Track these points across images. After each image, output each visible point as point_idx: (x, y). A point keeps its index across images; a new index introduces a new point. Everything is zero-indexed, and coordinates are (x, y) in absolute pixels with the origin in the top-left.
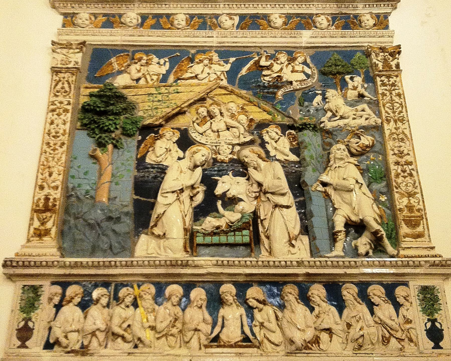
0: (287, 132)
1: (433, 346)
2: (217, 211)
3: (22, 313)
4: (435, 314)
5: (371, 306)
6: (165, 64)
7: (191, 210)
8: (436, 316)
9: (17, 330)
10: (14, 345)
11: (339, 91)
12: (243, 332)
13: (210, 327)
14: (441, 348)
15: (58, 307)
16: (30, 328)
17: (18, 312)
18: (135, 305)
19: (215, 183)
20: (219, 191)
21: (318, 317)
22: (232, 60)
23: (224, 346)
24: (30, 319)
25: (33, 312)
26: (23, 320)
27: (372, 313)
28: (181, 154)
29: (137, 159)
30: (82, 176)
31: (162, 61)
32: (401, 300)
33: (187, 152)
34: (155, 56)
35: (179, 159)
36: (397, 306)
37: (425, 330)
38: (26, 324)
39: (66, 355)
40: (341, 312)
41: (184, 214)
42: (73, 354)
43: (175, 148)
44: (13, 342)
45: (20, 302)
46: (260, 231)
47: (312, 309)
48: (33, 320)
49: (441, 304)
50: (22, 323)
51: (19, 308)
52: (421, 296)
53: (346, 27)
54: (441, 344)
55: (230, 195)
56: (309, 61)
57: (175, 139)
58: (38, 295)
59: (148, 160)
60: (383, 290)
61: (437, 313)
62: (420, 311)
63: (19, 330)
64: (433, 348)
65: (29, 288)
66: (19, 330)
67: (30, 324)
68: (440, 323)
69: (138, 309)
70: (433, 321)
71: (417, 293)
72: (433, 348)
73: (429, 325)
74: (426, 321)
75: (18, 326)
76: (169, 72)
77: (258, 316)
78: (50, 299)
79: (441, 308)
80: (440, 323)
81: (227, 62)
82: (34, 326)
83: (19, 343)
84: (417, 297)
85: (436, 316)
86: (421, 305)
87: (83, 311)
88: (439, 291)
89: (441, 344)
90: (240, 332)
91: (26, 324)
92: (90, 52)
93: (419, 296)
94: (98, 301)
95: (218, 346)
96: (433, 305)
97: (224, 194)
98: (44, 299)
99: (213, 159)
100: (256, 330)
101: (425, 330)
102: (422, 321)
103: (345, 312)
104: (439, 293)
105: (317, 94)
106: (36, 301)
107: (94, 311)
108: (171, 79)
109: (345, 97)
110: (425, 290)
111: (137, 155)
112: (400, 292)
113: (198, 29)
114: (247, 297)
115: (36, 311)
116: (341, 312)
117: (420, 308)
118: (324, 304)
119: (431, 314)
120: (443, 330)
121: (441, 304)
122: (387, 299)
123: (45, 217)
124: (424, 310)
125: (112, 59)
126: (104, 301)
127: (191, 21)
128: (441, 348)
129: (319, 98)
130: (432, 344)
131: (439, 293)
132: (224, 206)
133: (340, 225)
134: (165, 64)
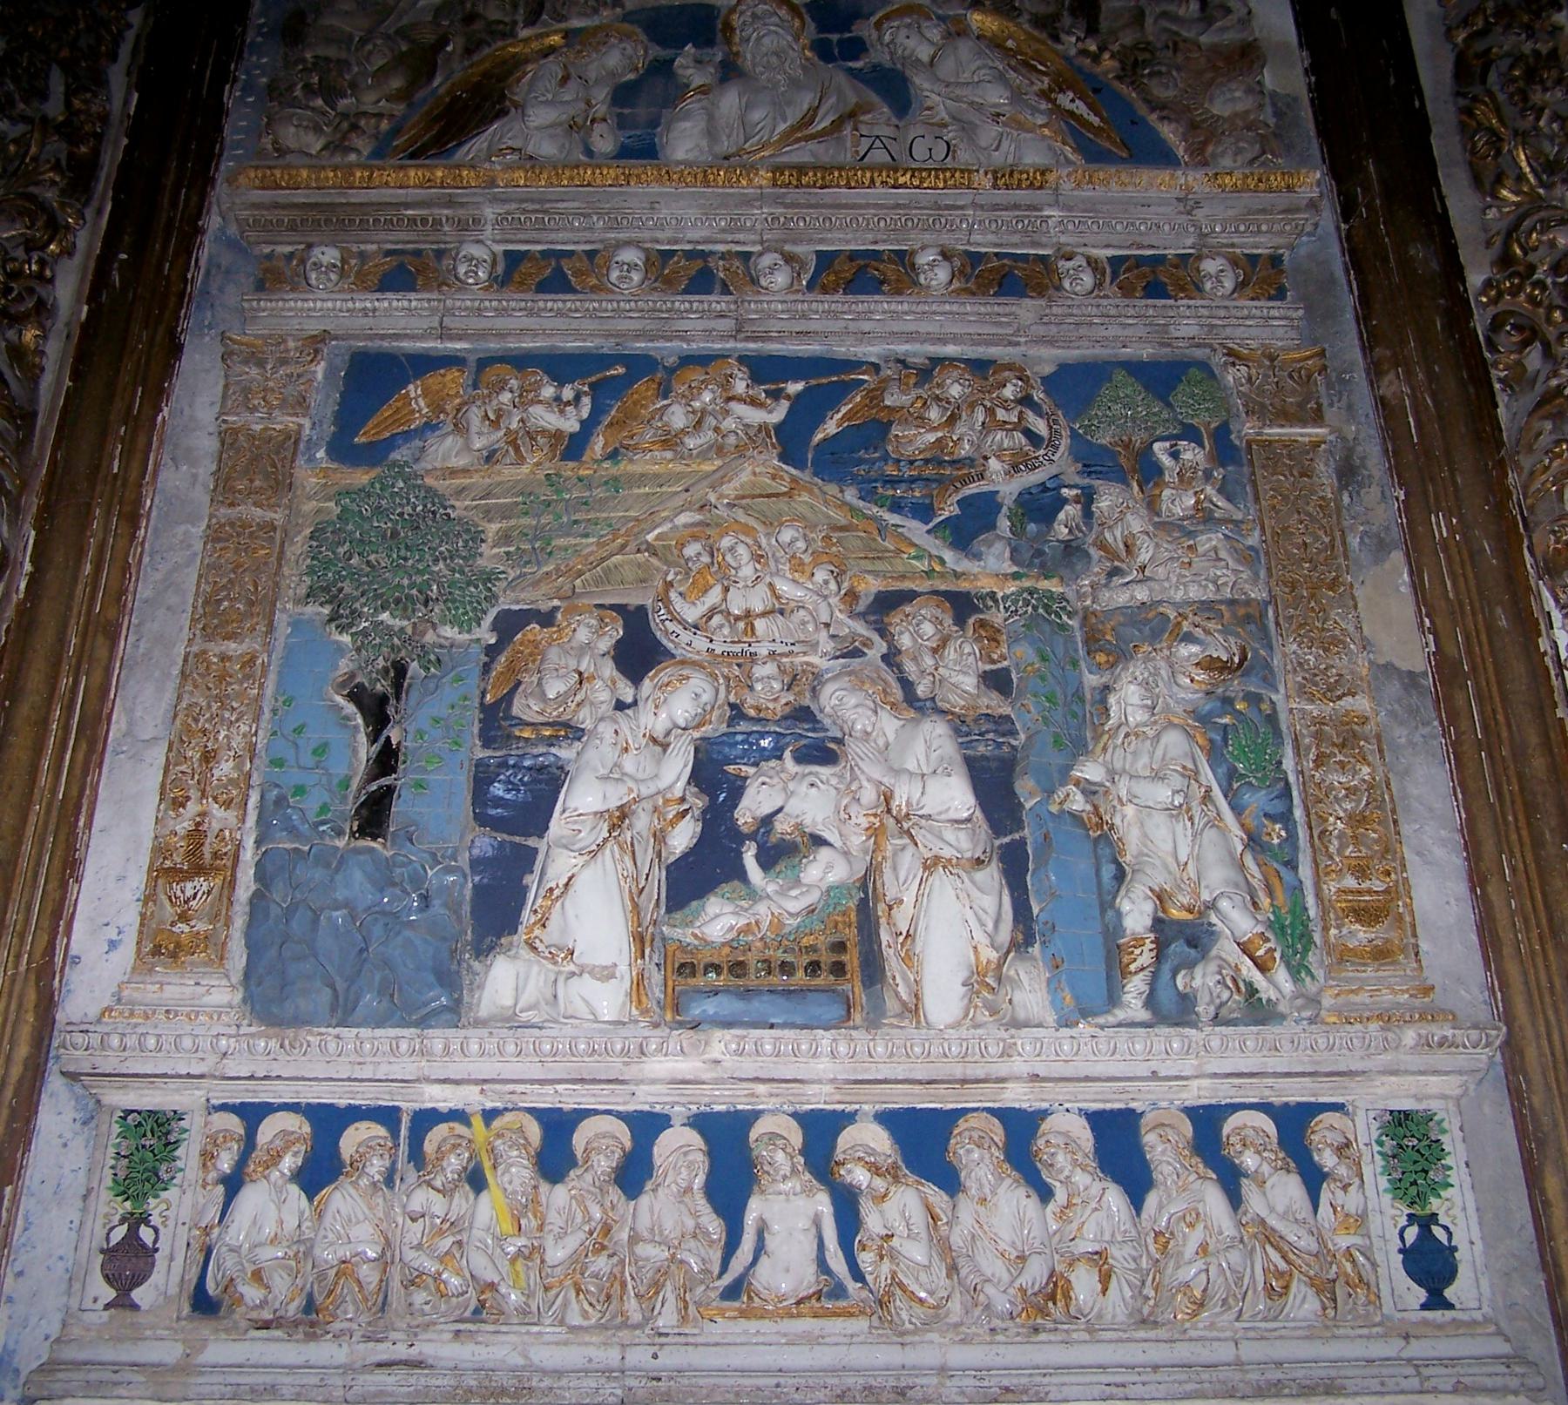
0: (971, 621)
1: (1423, 1300)
2: (742, 875)
3: (120, 1199)
4: (1432, 1199)
5: (1231, 1180)
6: (577, 398)
7: (659, 875)
8: (1435, 1204)
9: (102, 1251)
10: (95, 1300)
11: (1136, 488)
12: (822, 1265)
13: (716, 1256)
14: (1450, 1306)
15: (233, 1184)
16: (144, 1246)
17: (106, 1195)
18: (476, 1180)
19: (737, 789)
20: (748, 811)
21: (1063, 1214)
22: (794, 388)
23: (763, 1315)
24: (144, 1219)
25: (156, 1196)
26: (122, 1221)
27: (1235, 1199)
28: (627, 694)
29: (483, 707)
30: (308, 759)
31: (568, 393)
32: (1327, 1160)
33: (647, 684)
34: (546, 379)
35: (620, 706)
36: (1313, 1179)
37: (1400, 1251)
38: (133, 1233)
39: (263, 1333)
40: (1137, 1201)
41: (634, 890)
42: (278, 1333)
43: (609, 669)
44: (91, 1292)
45: (113, 1162)
46: (884, 944)
47: (1045, 1194)
48: (155, 1220)
49: (1450, 1168)
50: (122, 1231)
51: (110, 1183)
52: (1389, 1144)
53: (1155, 290)
54: (1449, 1293)
55: (782, 826)
56: (1038, 395)
57: (605, 644)
58: (168, 1144)
59: (516, 710)
60: (1270, 1127)
61: (1439, 1196)
62: (1385, 1191)
63: (110, 1253)
64: (1424, 1307)
65: (139, 1118)
66: (110, 1253)
67: (146, 1234)
68: (1446, 1228)
69: (484, 1195)
70: (1426, 1222)
71: (1375, 1135)
72: (1424, 1307)
73: (1412, 1233)
74: (1403, 1221)
75: (108, 1239)
76: (588, 426)
77: (873, 1222)
78: (208, 1157)
79: (1450, 1181)
80: (1446, 1228)
81: (776, 395)
82: (155, 1241)
83: (110, 1294)
84: (1377, 1148)
85: (1435, 1204)
86: (1387, 1170)
87: (310, 1199)
88: (1445, 1125)
89: (1449, 1293)
90: (813, 1268)
91: (133, 1233)
92: (342, 364)
93: (1381, 1144)
94: (358, 1165)
95: (744, 1314)
96: (1426, 1172)
97: (767, 821)
98: (188, 1155)
99: (732, 706)
100: (866, 1259)
101: (1400, 1251)
102: (1389, 1223)
103: (1152, 1200)
104: (1444, 1131)
105: (1065, 501)
106: (161, 1161)
107: (342, 1199)
108: (598, 445)
109: (1152, 505)
110: (1400, 1122)
111: (483, 694)
112: (1323, 1135)
113: (686, 292)
114: (839, 1156)
115: (164, 1194)
116: (1137, 1201)
117: (1384, 1182)
118: (1081, 1179)
119: (1420, 1198)
120: (1455, 1249)
121: (1450, 1168)
122: (1281, 1155)
123: (189, 892)
124: (1399, 1189)
125: (411, 387)
126: (376, 1167)
127: (663, 268)
128: (1450, 1306)
129: (1071, 511)
130: (1421, 1294)
131: (1444, 1131)
132: (768, 860)
133: (1136, 915)
134: (577, 398)
